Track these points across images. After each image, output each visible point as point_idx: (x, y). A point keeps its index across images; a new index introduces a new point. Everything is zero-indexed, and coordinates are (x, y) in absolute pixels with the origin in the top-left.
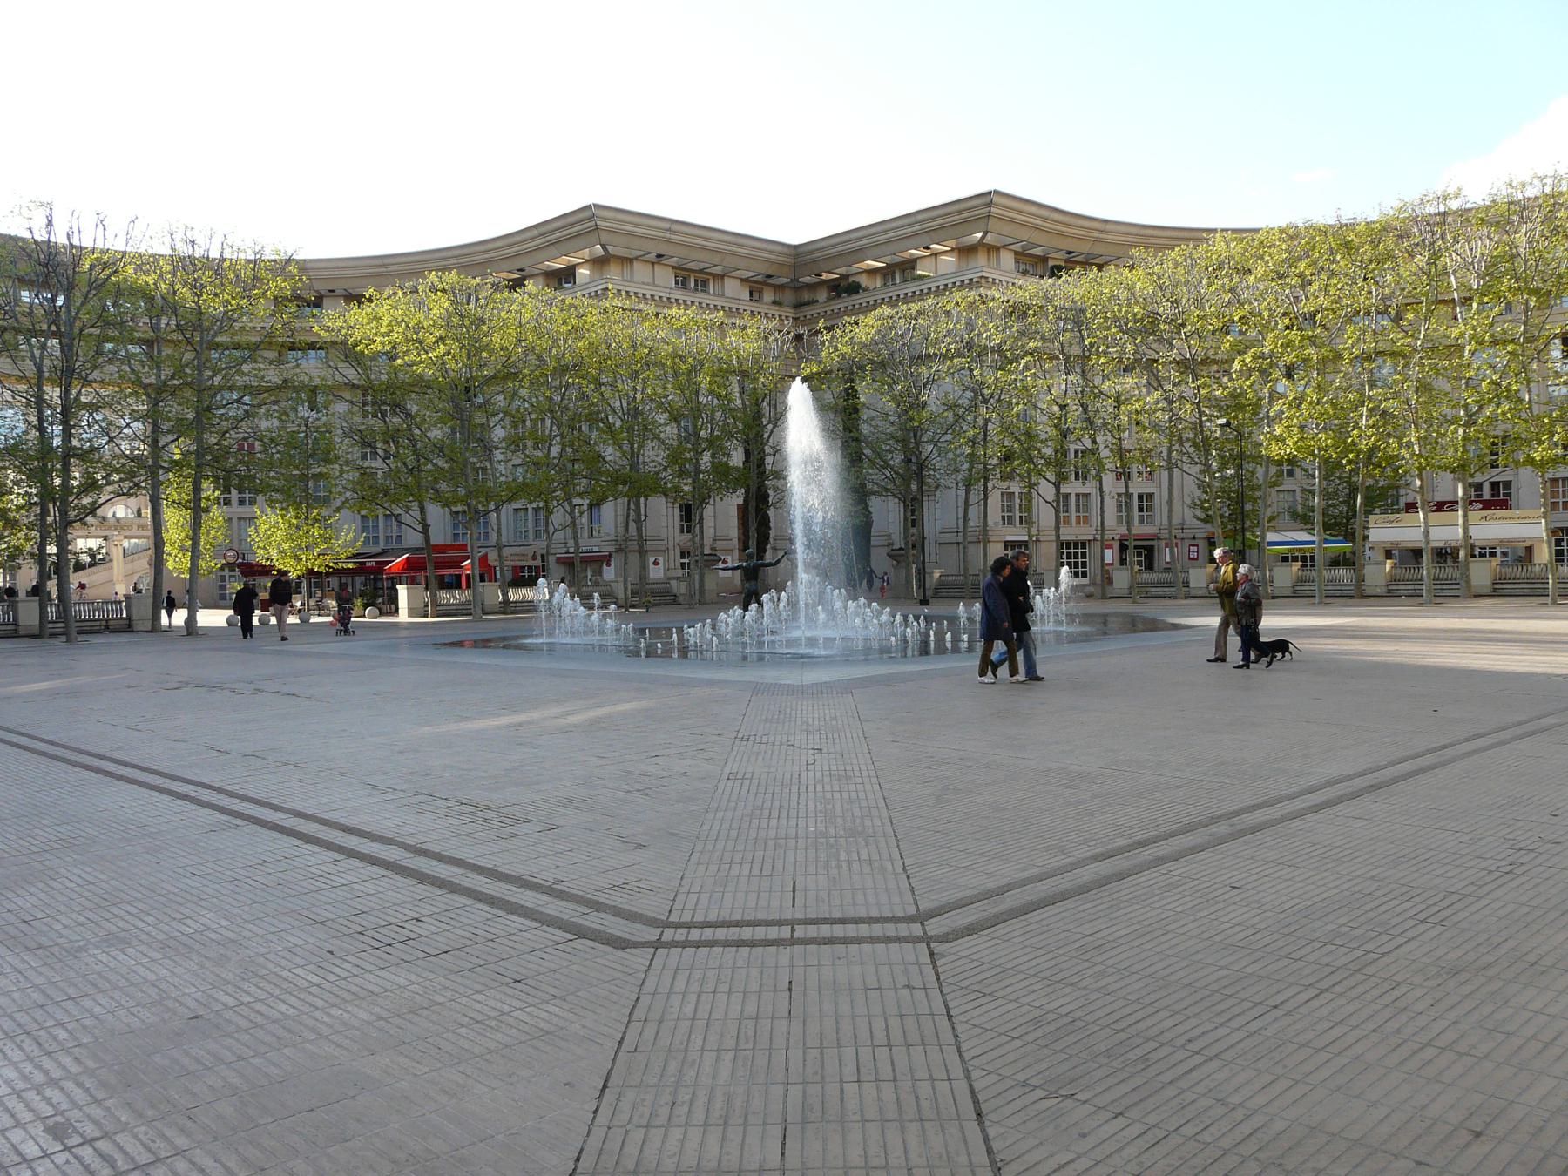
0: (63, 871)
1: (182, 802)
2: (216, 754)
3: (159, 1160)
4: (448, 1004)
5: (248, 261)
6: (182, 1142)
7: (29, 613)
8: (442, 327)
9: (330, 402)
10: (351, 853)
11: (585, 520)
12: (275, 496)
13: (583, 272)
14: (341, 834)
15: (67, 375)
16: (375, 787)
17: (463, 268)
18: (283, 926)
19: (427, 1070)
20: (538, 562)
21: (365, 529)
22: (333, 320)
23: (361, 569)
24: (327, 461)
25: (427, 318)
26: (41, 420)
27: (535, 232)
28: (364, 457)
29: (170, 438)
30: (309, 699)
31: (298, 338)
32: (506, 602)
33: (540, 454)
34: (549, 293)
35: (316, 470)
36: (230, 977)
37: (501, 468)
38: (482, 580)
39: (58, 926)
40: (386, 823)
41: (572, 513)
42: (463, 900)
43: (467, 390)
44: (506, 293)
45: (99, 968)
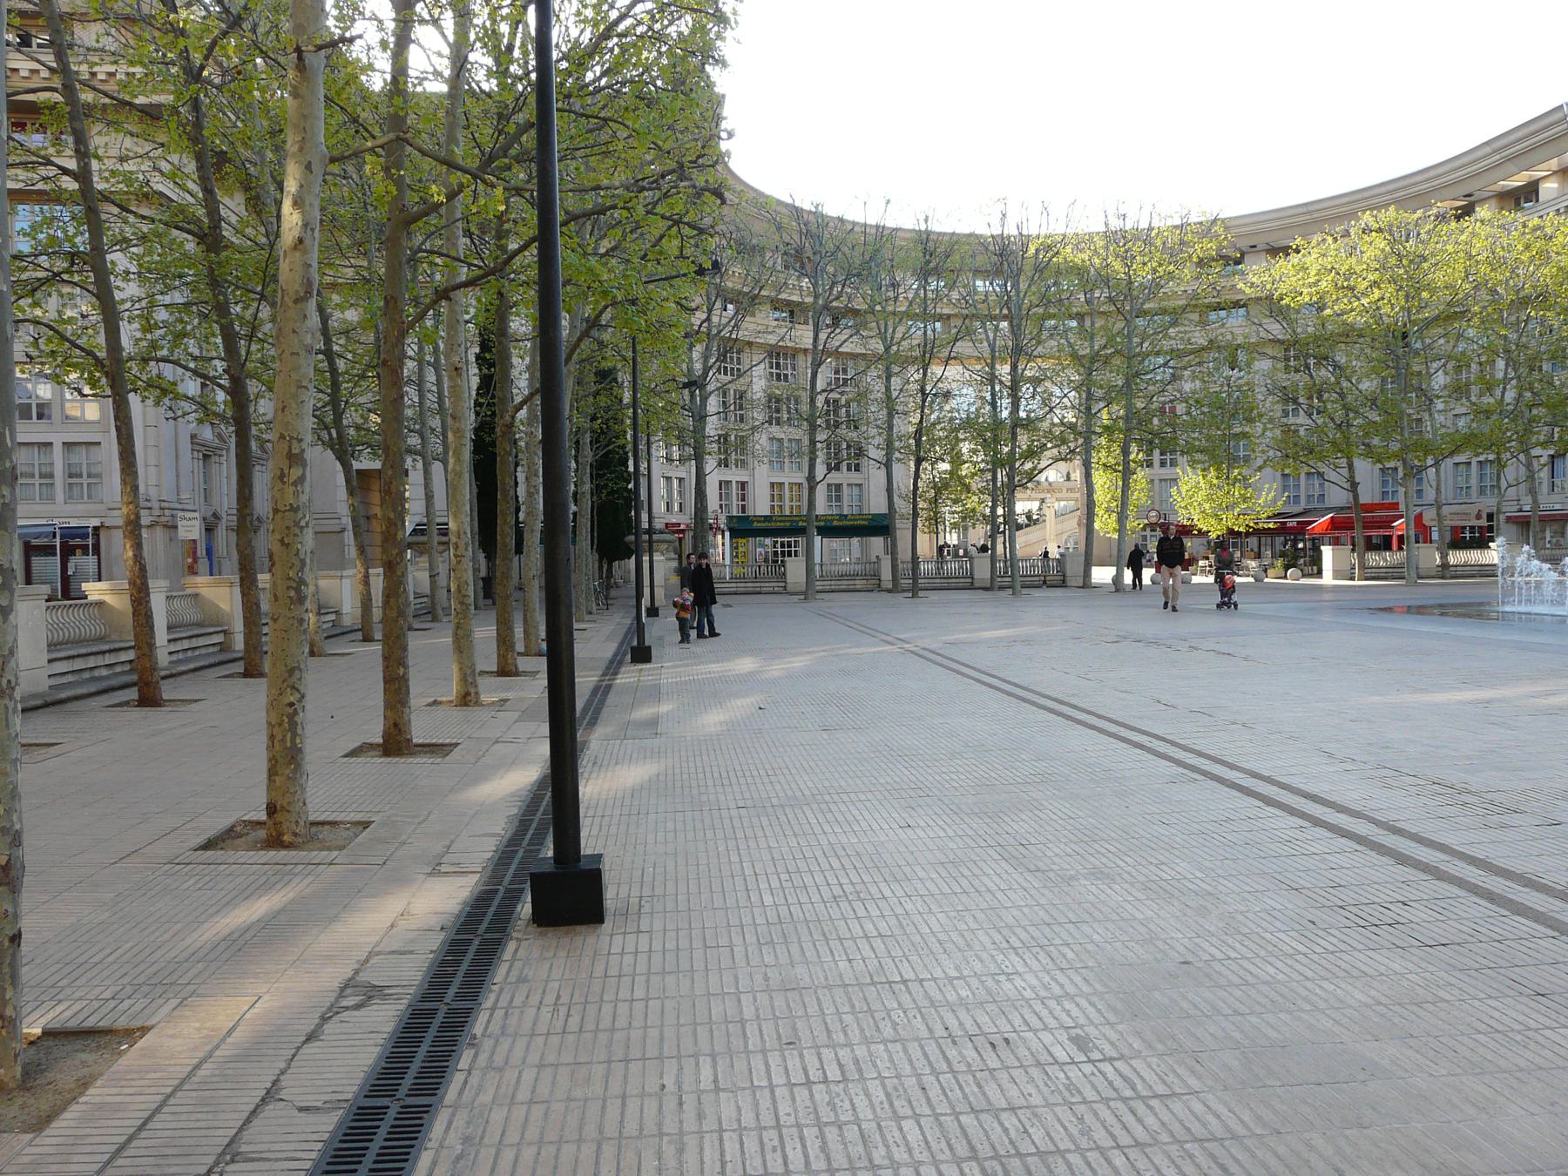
0: (1046, 804)
1: (1139, 751)
2: (1164, 707)
3: (1174, 1094)
4: (1457, 1003)
5: (1176, 227)
6: (1194, 1083)
7: (982, 570)
8: (1376, 270)
9: (1253, 359)
10: (1317, 822)
11: (1544, 474)
12: (1198, 456)
13: (1549, 188)
14: (1303, 800)
15: (1017, 353)
16: (1331, 755)
17: (1399, 203)
18: (1257, 887)
19: (1444, 1072)
20: (1484, 522)
21: (1285, 488)
22: (1256, 276)
23: (1282, 530)
24: (1250, 420)
25: (1359, 262)
26: (993, 395)
27: (1488, 150)
28: (1286, 413)
29: (1102, 404)
30: (1245, 659)
31: (1223, 298)
32: (1445, 566)
33: (1492, 400)
34: (1509, 216)
35: (1237, 430)
36: (1212, 929)
37: (1440, 418)
38: (1417, 542)
39: (1049, 854)
40: (1351, 795)
41: (1529, 465)
42: (1456, 891)
43: (1405, 336)
44: (1453, 224)
45: (1091, 898)
